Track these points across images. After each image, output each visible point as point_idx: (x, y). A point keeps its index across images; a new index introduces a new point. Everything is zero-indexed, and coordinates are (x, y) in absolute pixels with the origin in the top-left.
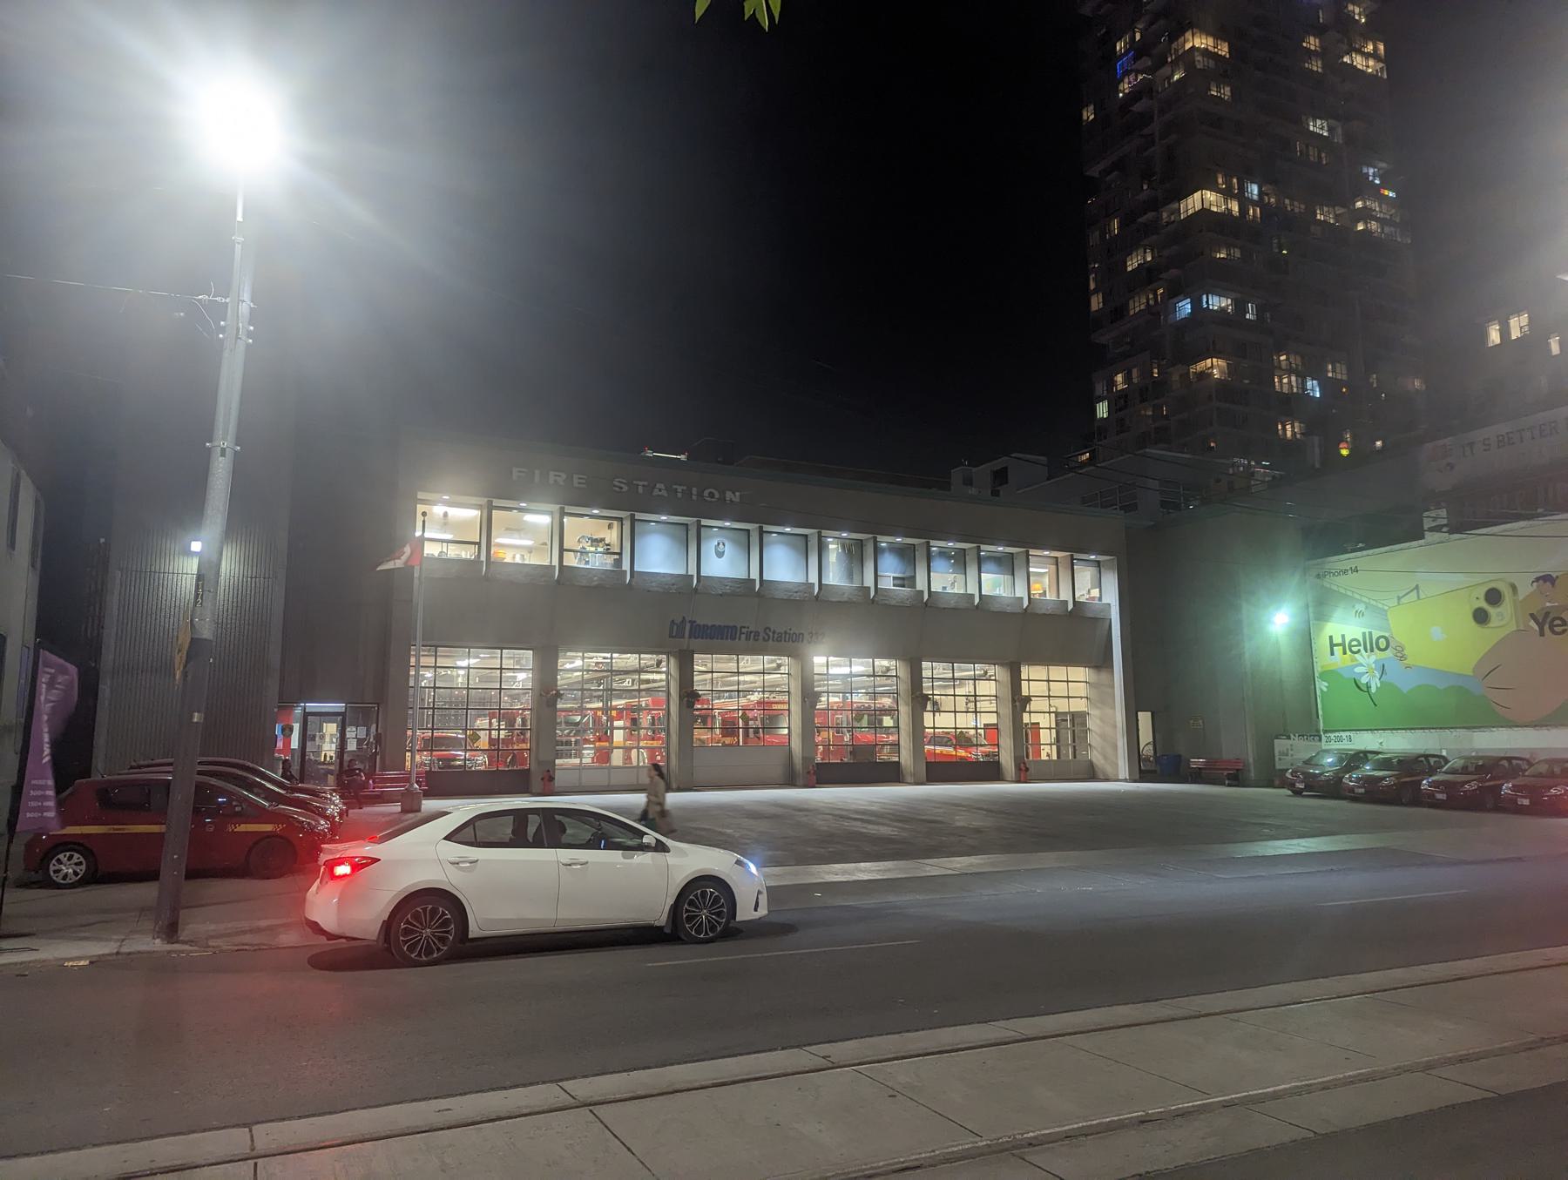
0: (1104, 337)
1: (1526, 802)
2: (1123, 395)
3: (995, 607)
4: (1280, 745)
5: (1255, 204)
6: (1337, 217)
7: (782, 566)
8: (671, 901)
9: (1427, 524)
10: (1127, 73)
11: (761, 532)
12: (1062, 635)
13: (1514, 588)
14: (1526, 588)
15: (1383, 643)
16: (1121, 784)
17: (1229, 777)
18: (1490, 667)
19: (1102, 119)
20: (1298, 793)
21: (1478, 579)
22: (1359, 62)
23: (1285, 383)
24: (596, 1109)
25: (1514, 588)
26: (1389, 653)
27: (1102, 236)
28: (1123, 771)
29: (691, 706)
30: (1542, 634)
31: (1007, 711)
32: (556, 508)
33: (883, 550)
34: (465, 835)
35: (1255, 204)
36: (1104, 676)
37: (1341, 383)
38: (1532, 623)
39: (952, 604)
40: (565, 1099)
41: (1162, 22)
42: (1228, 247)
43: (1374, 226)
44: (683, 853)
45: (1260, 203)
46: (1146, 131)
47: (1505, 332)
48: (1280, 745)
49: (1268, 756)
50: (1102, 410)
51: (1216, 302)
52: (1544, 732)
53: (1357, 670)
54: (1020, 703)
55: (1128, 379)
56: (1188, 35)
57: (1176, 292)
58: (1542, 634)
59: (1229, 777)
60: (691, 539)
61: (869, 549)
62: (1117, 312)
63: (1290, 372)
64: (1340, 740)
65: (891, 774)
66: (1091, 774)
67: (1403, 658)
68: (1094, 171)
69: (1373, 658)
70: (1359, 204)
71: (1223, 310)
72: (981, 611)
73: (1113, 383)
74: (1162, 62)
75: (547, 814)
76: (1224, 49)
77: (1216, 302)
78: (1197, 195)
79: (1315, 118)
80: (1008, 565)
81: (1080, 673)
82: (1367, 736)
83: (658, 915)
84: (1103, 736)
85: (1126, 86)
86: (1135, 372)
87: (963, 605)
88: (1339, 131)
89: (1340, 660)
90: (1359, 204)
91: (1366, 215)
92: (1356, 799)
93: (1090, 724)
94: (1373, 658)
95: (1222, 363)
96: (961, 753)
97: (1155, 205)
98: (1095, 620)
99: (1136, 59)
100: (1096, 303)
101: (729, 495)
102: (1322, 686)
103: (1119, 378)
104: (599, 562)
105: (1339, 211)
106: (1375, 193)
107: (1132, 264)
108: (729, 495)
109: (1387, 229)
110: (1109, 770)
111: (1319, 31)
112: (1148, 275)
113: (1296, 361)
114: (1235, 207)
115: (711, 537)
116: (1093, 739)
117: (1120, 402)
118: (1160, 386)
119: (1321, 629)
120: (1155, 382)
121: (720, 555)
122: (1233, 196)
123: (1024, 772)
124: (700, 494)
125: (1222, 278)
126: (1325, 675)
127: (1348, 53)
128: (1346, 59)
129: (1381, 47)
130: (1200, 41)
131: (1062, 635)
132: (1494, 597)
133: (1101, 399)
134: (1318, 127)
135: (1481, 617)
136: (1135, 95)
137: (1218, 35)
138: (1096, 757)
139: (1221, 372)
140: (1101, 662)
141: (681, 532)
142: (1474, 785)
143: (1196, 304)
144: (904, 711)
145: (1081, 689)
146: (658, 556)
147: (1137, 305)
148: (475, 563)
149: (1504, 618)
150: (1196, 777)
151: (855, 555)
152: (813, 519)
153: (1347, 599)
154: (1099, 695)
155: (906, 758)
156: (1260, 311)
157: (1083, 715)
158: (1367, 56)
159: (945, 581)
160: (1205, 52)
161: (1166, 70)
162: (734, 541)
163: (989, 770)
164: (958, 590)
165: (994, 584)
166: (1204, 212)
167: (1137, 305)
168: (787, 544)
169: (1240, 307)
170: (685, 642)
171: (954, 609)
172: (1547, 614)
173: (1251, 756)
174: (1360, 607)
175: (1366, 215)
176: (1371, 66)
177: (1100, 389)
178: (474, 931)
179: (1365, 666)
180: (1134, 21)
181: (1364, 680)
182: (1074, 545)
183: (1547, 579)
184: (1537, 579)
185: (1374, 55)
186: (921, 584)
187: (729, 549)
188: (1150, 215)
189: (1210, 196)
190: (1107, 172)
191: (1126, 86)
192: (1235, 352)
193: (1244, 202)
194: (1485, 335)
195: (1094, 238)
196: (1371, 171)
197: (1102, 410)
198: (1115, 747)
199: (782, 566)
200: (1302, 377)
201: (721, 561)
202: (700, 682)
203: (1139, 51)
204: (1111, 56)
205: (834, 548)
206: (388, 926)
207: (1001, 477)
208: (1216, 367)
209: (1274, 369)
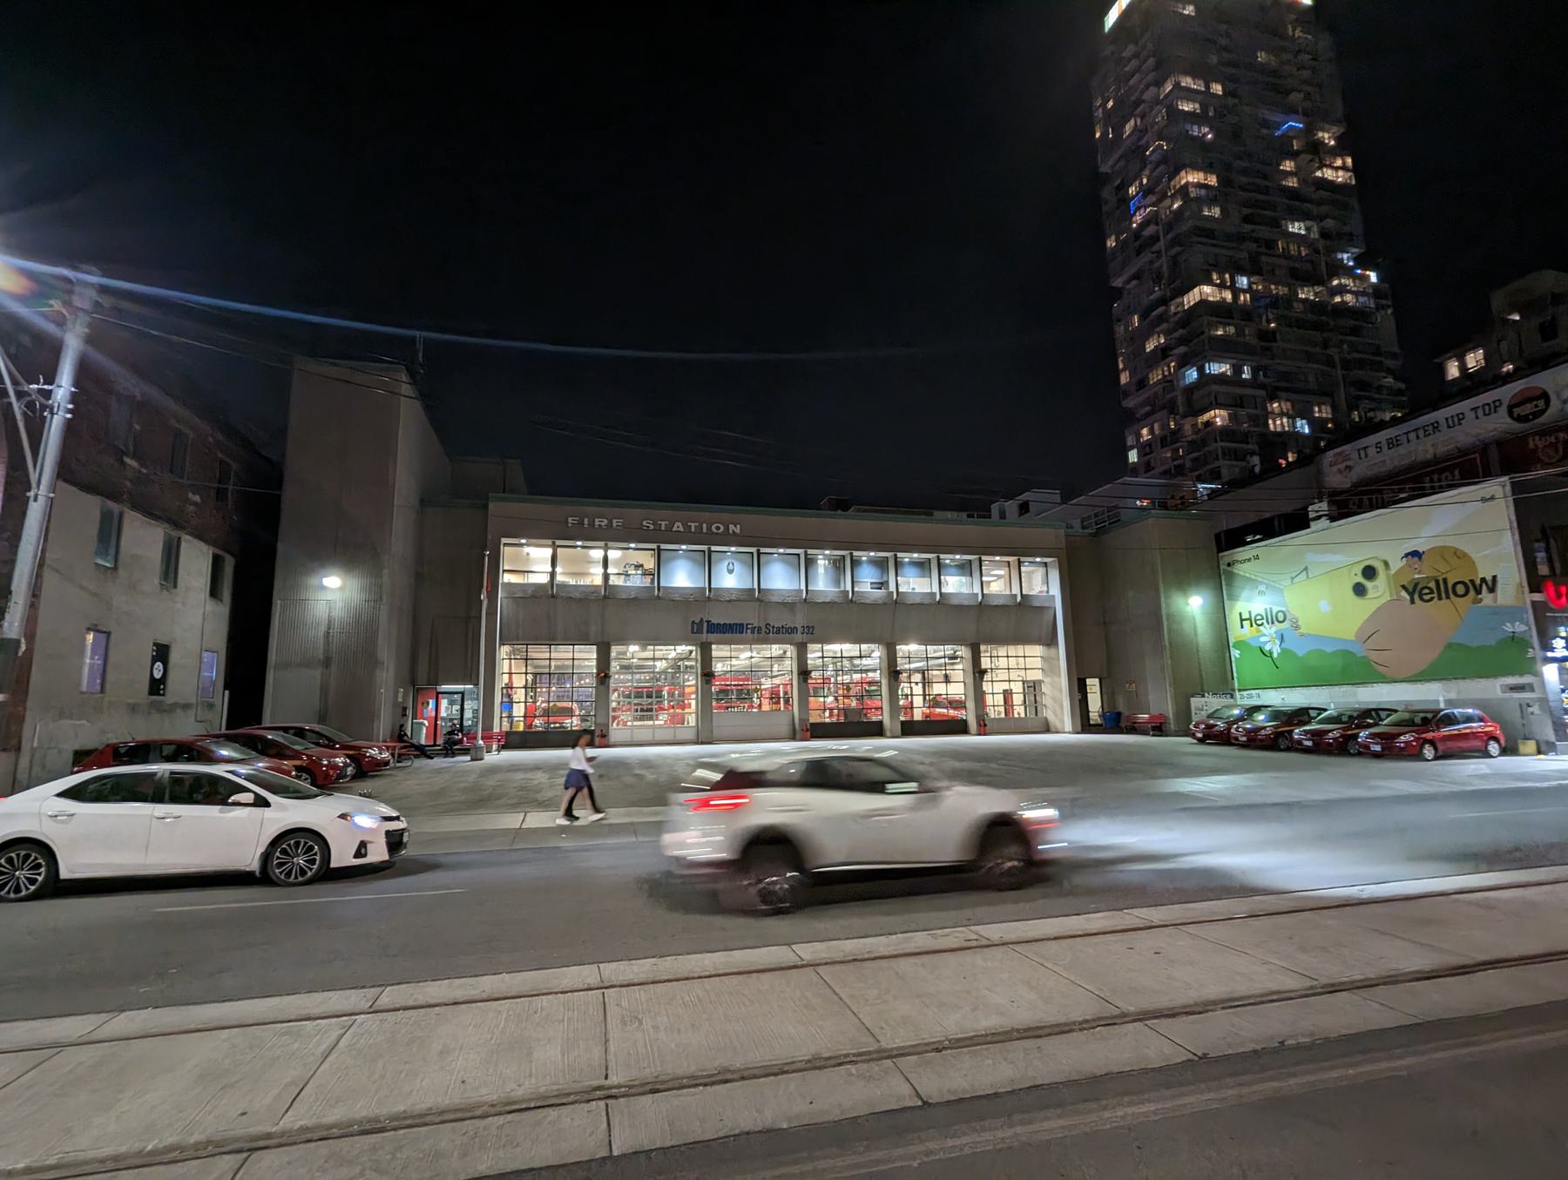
0: (1129, 403)
1: (1378, 748)
2: (1149, 444)
3: (955, 601)
4: (1196, 702)
5: (1245, 291)
6: (1316, 294)
7: (780, 578)
8: (261, 849)
9: (1312, 515)
10: (1138, 208)
11: (1020, 563)
12: (1013, 622)
13: (1386, 564)
14: (1397, 564)
15: (1281, 617)
16: (1066, 735)
17: (1154, 729)
18: (1368, 634)
19: (1122, 245)
20: (1201, 741)
21: (1339, 559)
22: (1329, 174)
23: (1277, 424)
24: (821, 970)
25: (1386, 564)
26: (1286, 625)
27: (1126, 329)
28: (1068, 726)
29: (805, 680)
30: (1413, 602)
31: (970, 680)
32: (549, 542)
33: (947, 566)
34: (73, 794)
35: (1245, 291)
36: (1053, 651)
37: (1326, 421)
38: (1404, 594)
39: (918, 600)
40: (793, 959)
41: (1161, 168)
42: (1225, 325)
43: (1349, 298)
44: (284, 808)
45: (1249, 290)
46: (1154, 248)
47: (1463, 367)
48: (1196, 702)
49: (1185, 713)
50: (1133, 456)
51: (1218, 368)
52: (1419, 686)
53: (1263, 639)
54: (979, 673)
55: (1151, 432)
56: (1183, 173)
57: (1184, 363)
58: (1413, 602)
59: (1154, 729)
60: (757, 564)
61: (975, 566)
62: (1141, 384)
63: (1282, 414)
64: (1251, 697)
65: (877, 730)
66: (1047, 728)
67: (1297, 628)
68: (1118, 283)
69: (1274, 629)
70: (1335, 282)
71: (1223, 374)
72: (942, 605)
73: (1139, 435)
74: (1164, 197)
75: (198, 778)
76: (1213, 180)
77: (1218, 368)
78: (1196, 290)
79: (1293, 221)
80: (965, 569)
81: (1037, 650)
82: (1272, 693)
83: (250, 860)
84: (1054, 699)
85: (1138, 218)
86: (1156, 426)
87: (927, 601)
88: (1315, 229)
89: (1247, 632)
90: (1335, 282)
91: (1342, 290)
92: (1244, 746)
93: (1044, 689)
94: (1274, 629)
95: (1224, 413)
96: (952, 712)
97: (1164, 301)
98: (1041, 609)
99: (1144, 197)
100: (1124, 378)
101: (732, 527)
102: (1235, 653)
103: (1145, 431)
104: (637, 581)
105: (1318, 289)
106: (1349, 272)
107: (1150, 346)
108: (732, 527)
109: (1361, 299)
110: (1059, 725)
111: (1293, 155)
112: (1163, 353)
113: (1286, 406)
114: (1228, 296)
115: (721, 560)
116: (1047, 700)
117: (1145, 449)
118: (1175, 435)
119: (1232, 608)
120: (1173, 433)
121: (731, 572)
122: (1226, 288)
123: (983, 728)
124: (709, 528)
125: (1223, 349)
126: (1238, 645)
127: (1320, 168)
128: (1319, 174)
129: (1349, 161)
130: (1192, 177)
131: (1013, 622)
132: (1369, 573)
133: (1132, 448)
134: (1296, 228)
135: (1359, 590)
136: (1143, 226)
137: (1207, 168)
138: (1048, 714)
139: (1223, 419)
140: (1051, 641)
141: (699, 556)
142: (1336, 734)
143: (1201, 370)
144: (884, 682)
145: (1038, 663)
146: (682, 576)
147: (1156, 376)
148: (650, 589)
149: (1380, 591)
150: (1132, 730)
151: (838, 566)
152: (803, 544)
153: (1252, 582)
154: (1049, 666)
155: (886, 719)
156: (1254, 371)
157: (1040, 682)
158: (1337, 169)
159: (914, 584)
160: (1199, 185)
161: (1167, 202)
162: (742, 562)
163: (960, 728)
164: (965, 590)
165: (955, 584)
166: (1203, 303)
167: (1156, 376)
168: (784, 561)
169: (1237, 370)
170: (705, 637)
171: (635, 599)
172: (1416, 585)
173: (1169, 710)
174: (1262, 588)
175: (1342, 290)
176: (1341, 177)
177: (1130, 441)
178: (65, 873)
179: (1268, 636)
180: (1142, 170)
181: (1267, 648)
182: (1019, 551)
183: (1415, 554)
184: (1407, 555)
185: (1344, 168)
186: (892, 588)
187: (737, 567)
188: (1162, 309)
189: (1207, 289)
190: (1128, 281)
191: (1138, 218)
192: (1234, 404)
193: (1236, 292)
194: (1442, 370)
195: (1120, 330)
196: (1345, 256)
197: (1133, 456)
198: (1062, 707)
199: (780, 578)
200: (1292, 418)
201: (731, 577)
202: (985, 663)
203: (1146, 192)
204: (1124, 200)
205: (822, 563)
206: (266, 857)
207: (1024, 508)
208: (1219, 417)
209: (1267, 415)
